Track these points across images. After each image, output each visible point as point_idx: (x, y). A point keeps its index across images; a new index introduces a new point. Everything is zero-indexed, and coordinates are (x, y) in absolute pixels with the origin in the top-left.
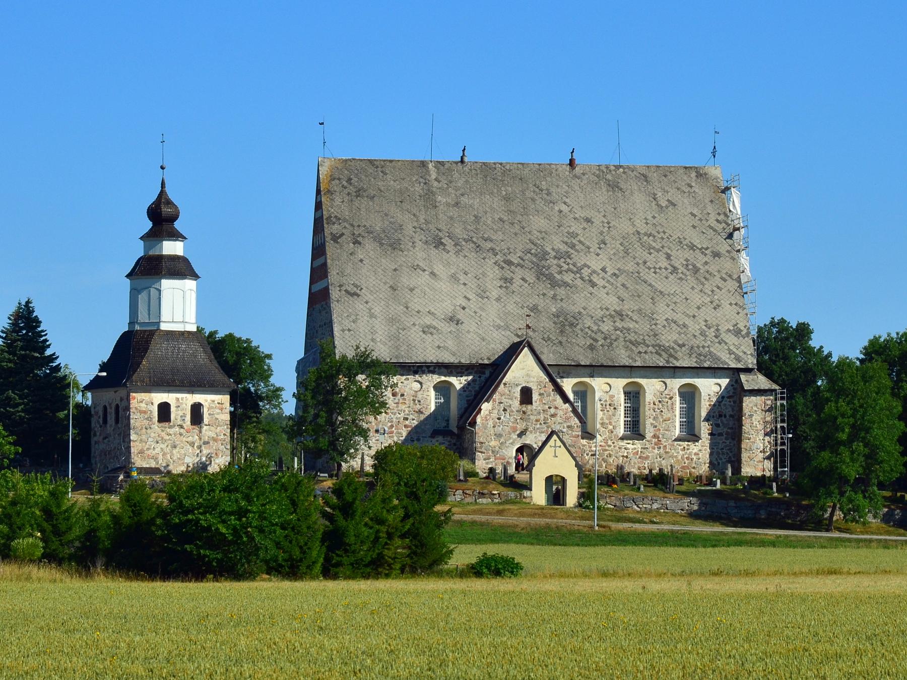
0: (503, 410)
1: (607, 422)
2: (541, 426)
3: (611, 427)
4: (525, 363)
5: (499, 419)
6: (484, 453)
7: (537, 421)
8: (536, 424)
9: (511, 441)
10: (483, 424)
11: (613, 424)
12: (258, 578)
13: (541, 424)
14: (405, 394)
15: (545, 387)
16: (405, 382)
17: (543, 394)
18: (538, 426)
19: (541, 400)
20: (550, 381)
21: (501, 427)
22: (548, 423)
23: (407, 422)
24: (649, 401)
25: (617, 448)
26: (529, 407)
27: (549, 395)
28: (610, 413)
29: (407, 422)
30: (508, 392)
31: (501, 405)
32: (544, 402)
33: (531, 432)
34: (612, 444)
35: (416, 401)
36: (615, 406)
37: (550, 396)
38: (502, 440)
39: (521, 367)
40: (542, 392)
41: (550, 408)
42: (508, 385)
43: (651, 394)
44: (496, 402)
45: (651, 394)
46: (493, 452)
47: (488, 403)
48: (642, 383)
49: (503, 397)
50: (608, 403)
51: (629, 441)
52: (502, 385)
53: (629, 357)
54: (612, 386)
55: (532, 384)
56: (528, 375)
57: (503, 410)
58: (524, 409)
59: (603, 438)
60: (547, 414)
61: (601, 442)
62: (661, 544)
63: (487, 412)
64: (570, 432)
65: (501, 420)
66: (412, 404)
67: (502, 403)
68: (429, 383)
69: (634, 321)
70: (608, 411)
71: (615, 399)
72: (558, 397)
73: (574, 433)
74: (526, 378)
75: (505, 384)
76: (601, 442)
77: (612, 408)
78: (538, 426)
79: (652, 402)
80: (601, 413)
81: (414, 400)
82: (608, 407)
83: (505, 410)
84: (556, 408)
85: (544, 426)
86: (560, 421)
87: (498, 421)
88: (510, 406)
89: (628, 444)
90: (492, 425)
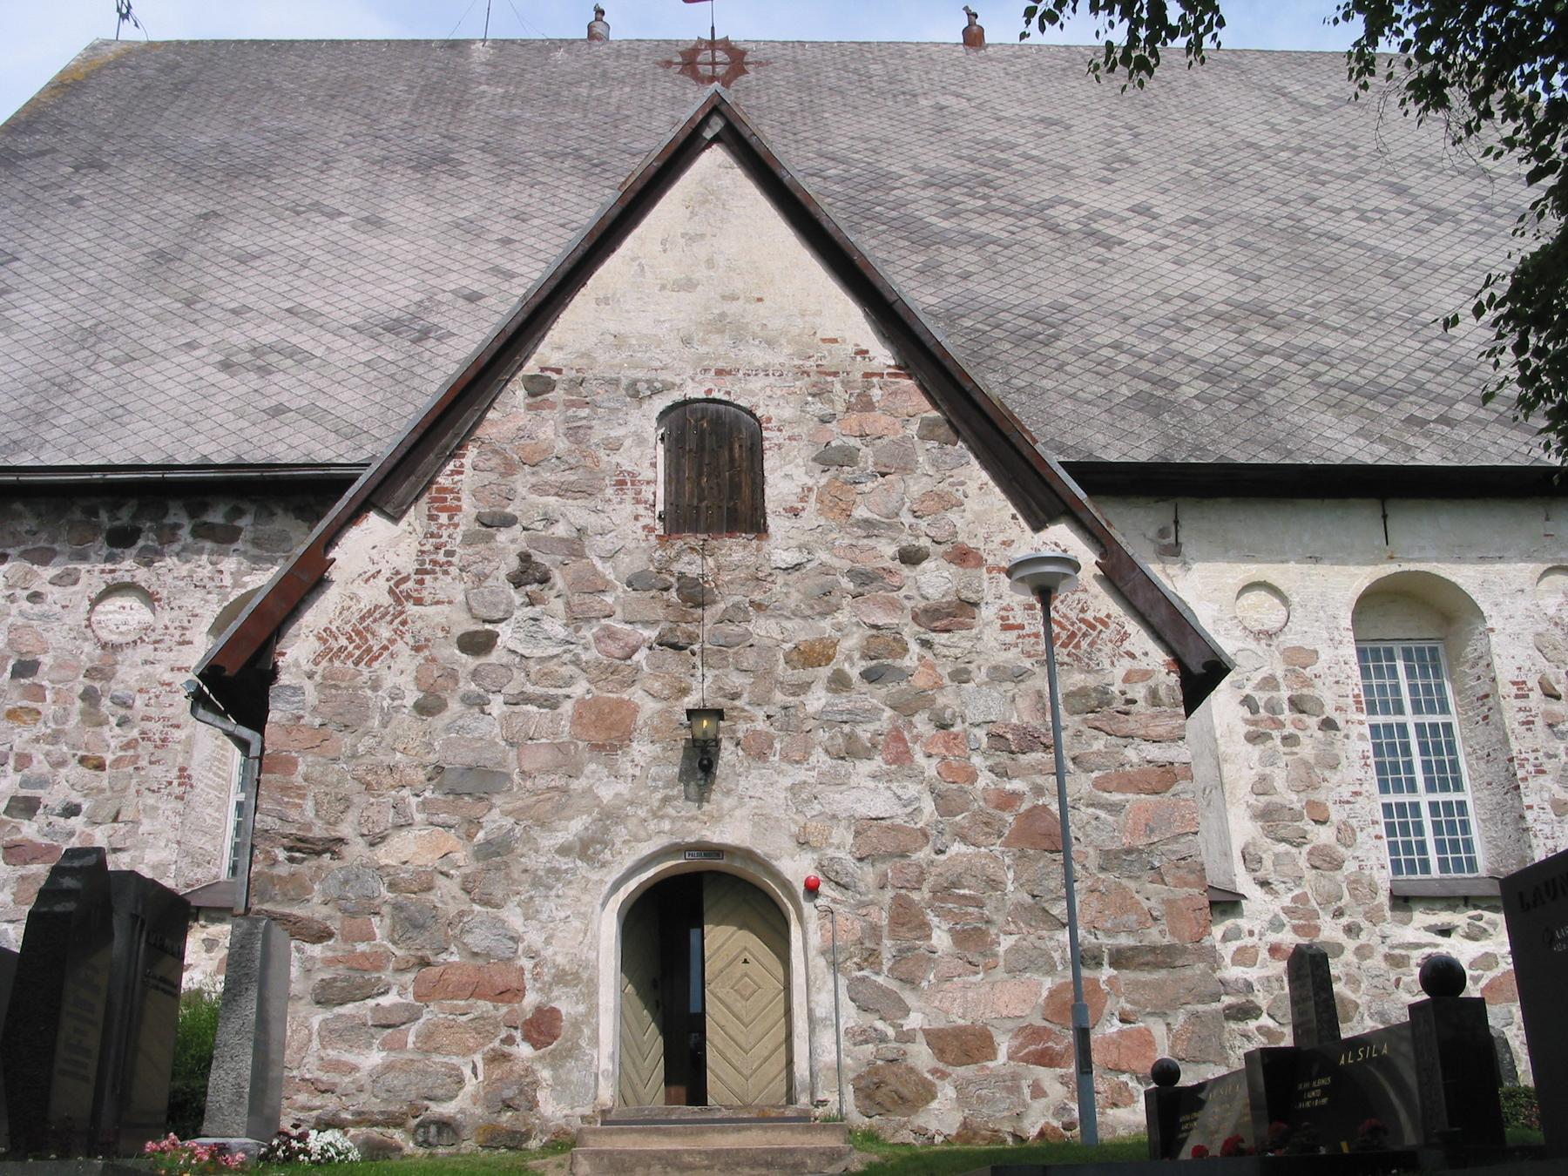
0: (518, 581)
1: (1294, 800)
2: (843, 702)
3: (1324, 836)
4: (701, 249)
5: (477, 643)
6: (323, 935)
7: (812, 655)
8: (804, 687)
9: (574, 827)
10: (329, 684)
11: (1336, 814)
12: (1248, 1110)
13: (839, 682)
14: (46, 660)
15: (867, 405)
16: (54, 594)
17: (846, 457)
18: (817, 699)
19: (837, 504)
20: (906, 367)
21: (497, 706)
22: (903, 674)
23: (30, 830)
24: (1513, 675)
25: (1377, 962)
26: (735, 550)
27: (895, 464)
28: (1307, 750)
29: (30, 830)
30: (562, 445)
31: (503, 536)
32: (860, 512)
33: (758, 751)
34: (1341, 938)
35: (106, 703)
36: (1329, 712)
37: (906, 467)
38: (495, 821)
39: (672, 272)
40: (837, 436)
41: (911, 557)
42: (557, 395)
43: (1516, 636)
44: (454, 511)
45: (1516, 636)
46: (410, 923)
47: (395, 519)
48: (1459, 581)
49: (522, 481)
50: (1284, 694)
51: (1444, 918)
52: (515, 394)
53: (1361, 433)
54: (1295, 599)
55: (756, 384)
56: (734, 329)
57: (518, 581)
58: (691, 566)
59: (1286, 900)
60: (893, 606)
61: (1276, 925)
62: (697, 1023)
63: (376, 594)
64: (1100, 744)
65: (496, 656)
66: (74, 719)
67: (508, 521)
68: (192, 600)
69: (1335, 329)
70: (1287, 739)
71: (1318, 668)
72: (975, 475)
73: (1131, 754)
74: (718, 347)
75: (539, 387)
76: (1276, 925)
77: (1313, 722)
78: (817, 699)
79: (1533, 682)
80: (1255, 752)
81: (90, 696)
82: (1287, 715)
83: (528, 574)
84: (963, 557)
85: (873, 696)
86: (1002, 657)
87: (470, 662)
88: (575, 546)
89: (1445, 932)
90: (412, 696)
